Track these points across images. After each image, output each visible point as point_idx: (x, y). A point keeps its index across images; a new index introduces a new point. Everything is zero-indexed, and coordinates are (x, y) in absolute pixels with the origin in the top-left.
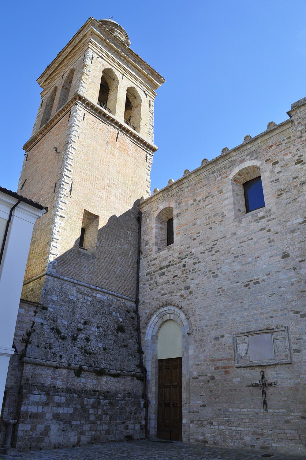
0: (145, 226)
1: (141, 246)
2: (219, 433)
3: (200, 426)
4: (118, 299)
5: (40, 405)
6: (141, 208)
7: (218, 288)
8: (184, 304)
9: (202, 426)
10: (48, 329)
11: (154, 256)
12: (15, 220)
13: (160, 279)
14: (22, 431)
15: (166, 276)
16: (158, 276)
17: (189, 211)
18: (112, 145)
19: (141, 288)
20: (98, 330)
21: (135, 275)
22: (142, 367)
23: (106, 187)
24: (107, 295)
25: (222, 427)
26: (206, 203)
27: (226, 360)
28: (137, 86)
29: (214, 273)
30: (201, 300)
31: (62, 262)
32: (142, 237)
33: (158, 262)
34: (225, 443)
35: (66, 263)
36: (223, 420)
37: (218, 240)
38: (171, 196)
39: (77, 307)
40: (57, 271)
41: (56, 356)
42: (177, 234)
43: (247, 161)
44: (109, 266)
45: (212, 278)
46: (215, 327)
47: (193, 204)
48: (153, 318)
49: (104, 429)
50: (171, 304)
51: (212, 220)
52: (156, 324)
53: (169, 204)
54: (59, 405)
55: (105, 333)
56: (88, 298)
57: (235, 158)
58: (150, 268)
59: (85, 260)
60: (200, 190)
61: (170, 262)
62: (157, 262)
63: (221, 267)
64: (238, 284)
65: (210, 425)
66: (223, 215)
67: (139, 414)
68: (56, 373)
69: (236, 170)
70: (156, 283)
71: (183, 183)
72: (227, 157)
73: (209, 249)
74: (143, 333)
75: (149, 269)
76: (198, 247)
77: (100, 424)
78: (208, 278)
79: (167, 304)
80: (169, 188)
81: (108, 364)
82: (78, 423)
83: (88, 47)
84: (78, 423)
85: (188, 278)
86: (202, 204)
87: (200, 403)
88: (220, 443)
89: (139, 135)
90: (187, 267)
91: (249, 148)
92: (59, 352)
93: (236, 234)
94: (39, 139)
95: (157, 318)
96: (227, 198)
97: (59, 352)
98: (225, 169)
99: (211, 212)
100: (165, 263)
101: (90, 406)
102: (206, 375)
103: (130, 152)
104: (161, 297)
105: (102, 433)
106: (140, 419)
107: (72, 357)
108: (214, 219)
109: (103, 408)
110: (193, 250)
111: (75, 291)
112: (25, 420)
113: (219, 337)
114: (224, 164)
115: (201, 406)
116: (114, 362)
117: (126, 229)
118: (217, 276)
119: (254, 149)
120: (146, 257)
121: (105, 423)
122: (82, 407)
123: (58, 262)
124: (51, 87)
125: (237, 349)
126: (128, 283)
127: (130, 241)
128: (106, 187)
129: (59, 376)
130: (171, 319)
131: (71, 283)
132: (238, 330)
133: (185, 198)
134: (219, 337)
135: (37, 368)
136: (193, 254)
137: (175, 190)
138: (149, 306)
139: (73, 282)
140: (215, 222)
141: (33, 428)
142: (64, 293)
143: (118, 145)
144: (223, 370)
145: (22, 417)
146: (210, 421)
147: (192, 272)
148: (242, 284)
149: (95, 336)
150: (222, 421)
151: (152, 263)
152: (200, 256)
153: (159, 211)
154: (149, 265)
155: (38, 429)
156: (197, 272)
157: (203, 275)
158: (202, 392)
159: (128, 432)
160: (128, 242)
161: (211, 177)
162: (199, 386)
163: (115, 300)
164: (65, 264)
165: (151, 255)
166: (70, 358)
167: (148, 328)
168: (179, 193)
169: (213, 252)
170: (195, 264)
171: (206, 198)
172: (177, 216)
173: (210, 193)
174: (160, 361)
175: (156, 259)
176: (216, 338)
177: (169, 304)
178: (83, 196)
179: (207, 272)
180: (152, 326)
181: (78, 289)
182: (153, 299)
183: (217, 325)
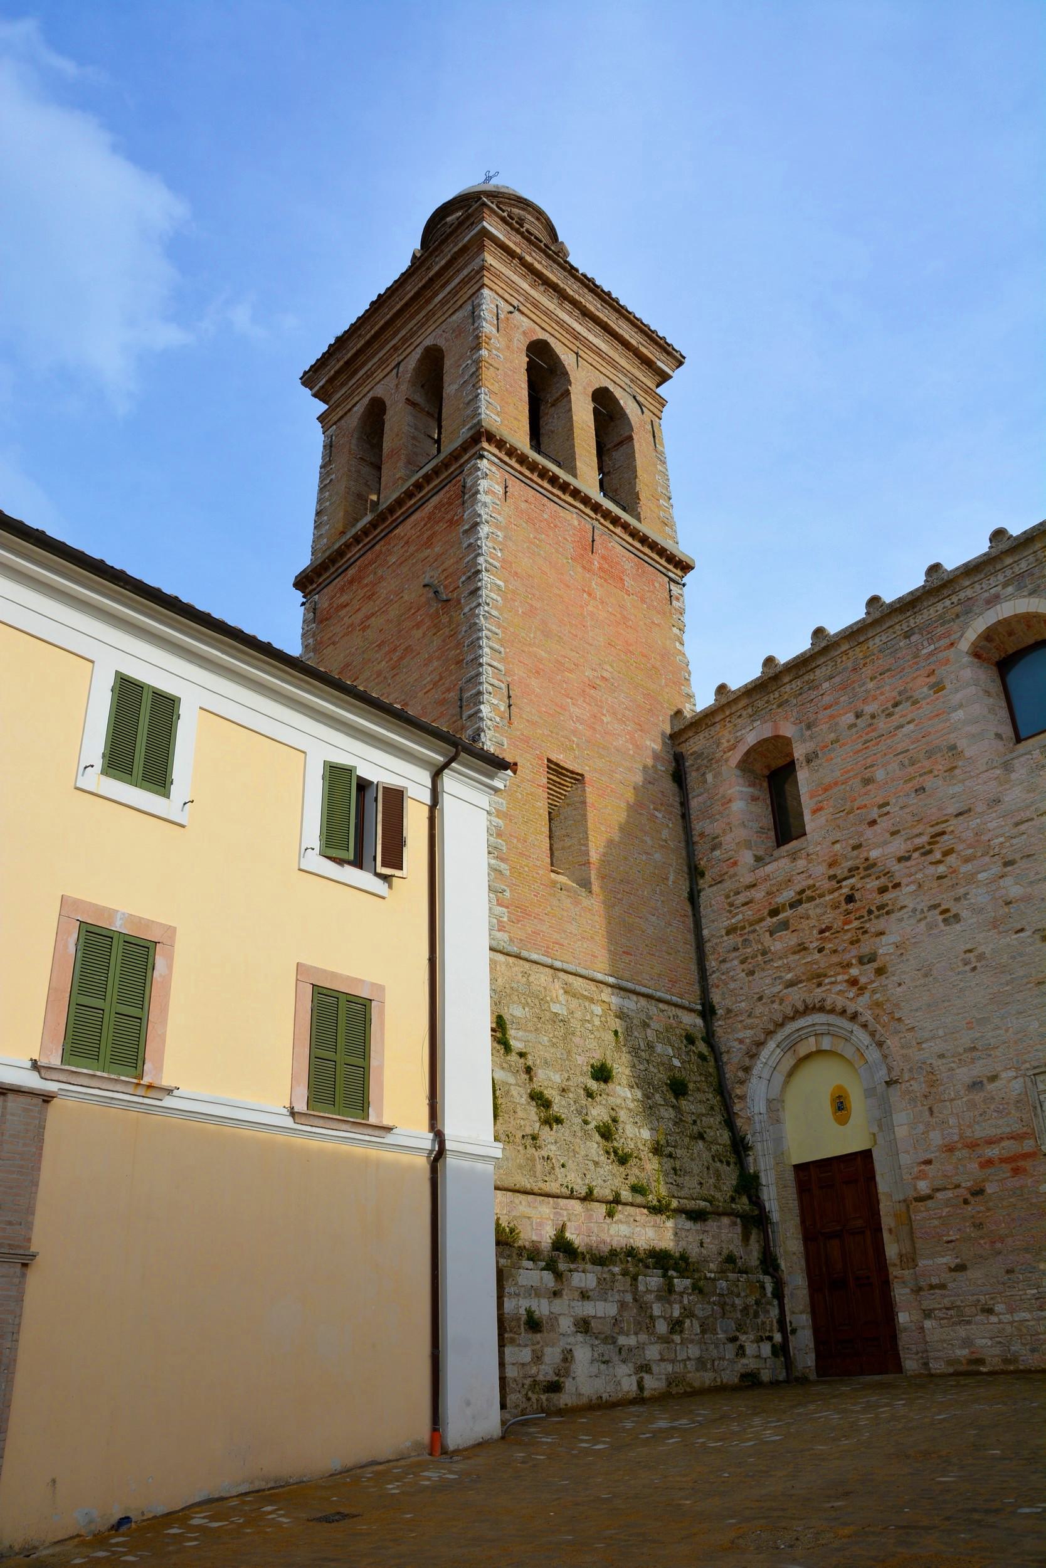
0: (702, 794)
1: (696, 853)
2: (1016, 1333)
3: (955, 1324)
4: (661, 1006)
5: (544, 1297)
6: (679, 744)
7: (965, 952)
8: (861, 1004)
9: (963, 1320)
10: (521, 1097)
11: (748, 879)
12: (447, 802)
13: (776, 943)
14: (513, 1364)
15: (793, 931)
16: (768, 933)
17: (844, 745)
18: (584, 567)
19: (714, 972)
20: (632, 1094)
21: (691, 937)
22: (749, 1185)
23: (587, 690)
24: (634, 998)
25: (1024, 1314)
26: (896, 720)
27: (1012, 1138)
28: (615, 383)
29: (947, 911)
30: (916, 987)
31: (518, 912)
32: (697, 826)
33: (763, 893)
34: (1036, 1355)
35: (527, 914)
36: (1023, 1297)
37: (947, 821)
38: (779, 706)
39: (573, 1034)
40: (510, 937)
41: (553, 1168)
42: (814, 812)
43: (1007, 601)
44: (628, 917)
45: (942, 924)
46: (968, 1057)
47: (854, 725)
48: (765, 1053)
49: (692, 1356)
50: (822, 1009)
51: (923, 767)
52: (775, 1068)
53: (776, 728)
54: (584, 1296)
55: (649, 1101)
56: (593, 1007)
57: (969, 593)
58: (737, 914)
59: (569, 901)
60: (871, 685)
61: (803, 891)
62: (758, 894)
63: (967, 894)
64: (1021, 934)
65: (986, 1314)
66: (954, 752)
67: (765, 1316)
68: (561, 1211)
69: (979, 625)
70: (764, 953)
71: (814, 665)
72: (946, 592)
73: (923, 847)
74: (740, 1097)
75: (733, 917)
76: (885, 843)
77: (681, 1343)
78: (931, 926)
79: (808, 1009)
80: (768, 683)
81: (672, 1184)
82: (632, 1341)
83: (479, 285)
84: (632, 1341)
85: (865, 932)
86: (882, 724)
87: (948, 1260)
88: (1022, 1358)
89: (644, 528)
90: (858, 902)
91: (1011, 565)
92: (559, 1157)
93: (999, 801)
94: (352, 560)
95: (778, 1050)
96: (961, 706)
97: (559, 1157)
98: (942, 625)
99: (915, 746)
100: (788, 895)
101: (653, 1296)
102: (958, 1186)
103: (628, 582)
104: (785, 991)
105: (689, 1366)
106: (768, 1328)
107: (590, 1168)
108: (927, 764)
109: (681, 1302)
110: (874, 854)
111: (561, 991)
112: (517, 1336)
113: (981, 1082)
114: (937, 611)
115: (951, 1270)
116: (686, 1178)
117: (652, 807)
118: (957, 918)
119: (1023, 565)
120: (720, 882)
121: (692, 1341)
122: (635, 1300)
123: (509, 912)
124: (357, 399)
125: (1041, 1106)
126: (679, 962)
127: (666, 841)
128: (587, 690)
129: (569, 1220)
130: (823, 1049)
131: (547, 969)
132: (1037, 1057)
133: (825, 709)
134: (981, 1082)
135: (517, 1201)
136: (874, 865)
137: (789, 688)
138: (750, 1021)
139: (551, 967)
140: (931, 772)
141: (538, 1358)
142: (537, 997)
143: (596, 563)
144: (1007, 1165)
145: (508, 1329)
146: (986, 1304)
147: (877, 913)
148: (1034, 933)
149: (630, 1110)
150: (1021, 1300)
151: (741, 898)
152: (896, 867)
153: (742, 749)
154: (731, 905)
155: (547, 1359)
156: (893, 912)
157: (913, 921)
158: (951, 1233)
159: (747, 1365)
160: (661, 843)
161: (900, 648)
162: (940, 1218)
163: (653, 1010)
164: (527, 918)
165: (735, 875)
166: (586, 1172)
167: (754, 1080)
168: (805, 696)
169: (938, 855)
170: (883, 890)
171: (896, 705)
172: (809, 761)
173: (905, 691)
174: (800, 1168)
175: (754, 885)
176: (976, 1085)
177: (814, 1008)
178: (538, 720)
179: (925, 909)
180: (766, 1074)
181: (566, 984)
182: (760, 999)
183: (974, 1049)
